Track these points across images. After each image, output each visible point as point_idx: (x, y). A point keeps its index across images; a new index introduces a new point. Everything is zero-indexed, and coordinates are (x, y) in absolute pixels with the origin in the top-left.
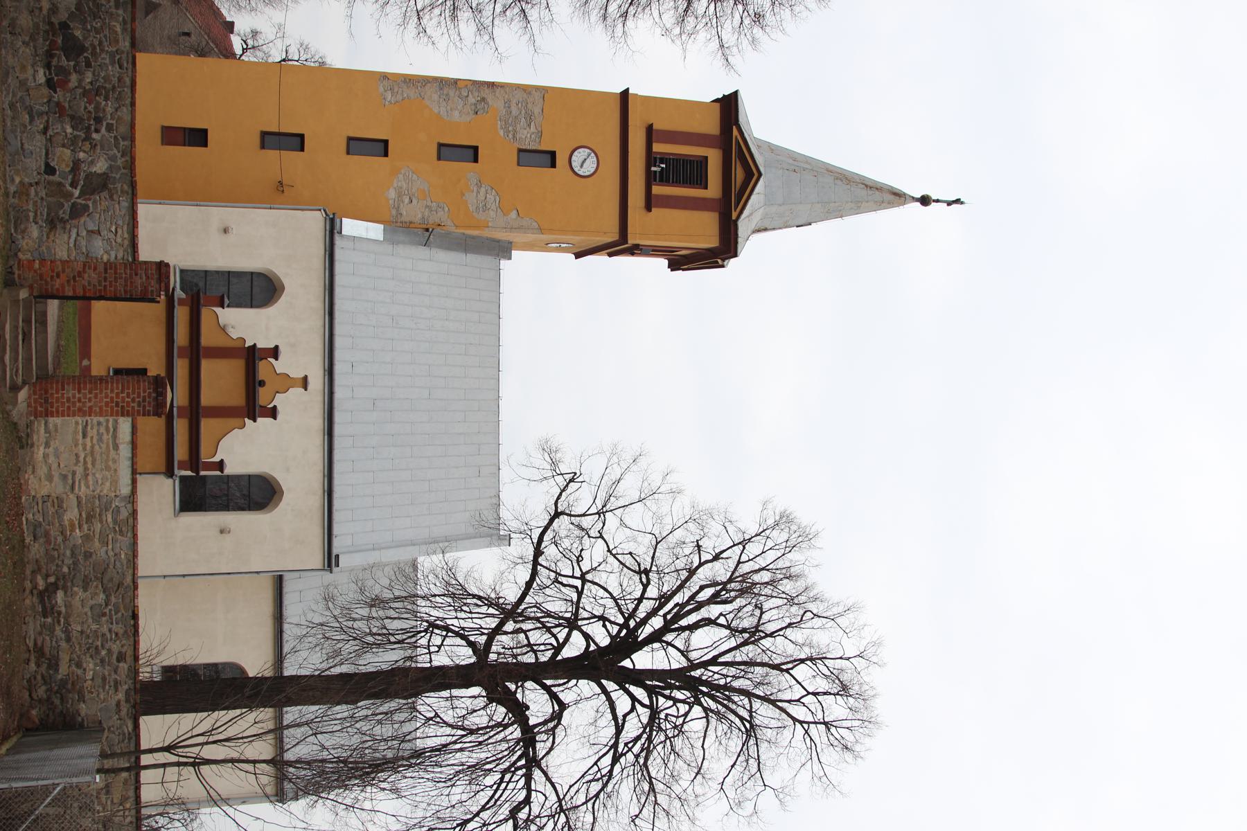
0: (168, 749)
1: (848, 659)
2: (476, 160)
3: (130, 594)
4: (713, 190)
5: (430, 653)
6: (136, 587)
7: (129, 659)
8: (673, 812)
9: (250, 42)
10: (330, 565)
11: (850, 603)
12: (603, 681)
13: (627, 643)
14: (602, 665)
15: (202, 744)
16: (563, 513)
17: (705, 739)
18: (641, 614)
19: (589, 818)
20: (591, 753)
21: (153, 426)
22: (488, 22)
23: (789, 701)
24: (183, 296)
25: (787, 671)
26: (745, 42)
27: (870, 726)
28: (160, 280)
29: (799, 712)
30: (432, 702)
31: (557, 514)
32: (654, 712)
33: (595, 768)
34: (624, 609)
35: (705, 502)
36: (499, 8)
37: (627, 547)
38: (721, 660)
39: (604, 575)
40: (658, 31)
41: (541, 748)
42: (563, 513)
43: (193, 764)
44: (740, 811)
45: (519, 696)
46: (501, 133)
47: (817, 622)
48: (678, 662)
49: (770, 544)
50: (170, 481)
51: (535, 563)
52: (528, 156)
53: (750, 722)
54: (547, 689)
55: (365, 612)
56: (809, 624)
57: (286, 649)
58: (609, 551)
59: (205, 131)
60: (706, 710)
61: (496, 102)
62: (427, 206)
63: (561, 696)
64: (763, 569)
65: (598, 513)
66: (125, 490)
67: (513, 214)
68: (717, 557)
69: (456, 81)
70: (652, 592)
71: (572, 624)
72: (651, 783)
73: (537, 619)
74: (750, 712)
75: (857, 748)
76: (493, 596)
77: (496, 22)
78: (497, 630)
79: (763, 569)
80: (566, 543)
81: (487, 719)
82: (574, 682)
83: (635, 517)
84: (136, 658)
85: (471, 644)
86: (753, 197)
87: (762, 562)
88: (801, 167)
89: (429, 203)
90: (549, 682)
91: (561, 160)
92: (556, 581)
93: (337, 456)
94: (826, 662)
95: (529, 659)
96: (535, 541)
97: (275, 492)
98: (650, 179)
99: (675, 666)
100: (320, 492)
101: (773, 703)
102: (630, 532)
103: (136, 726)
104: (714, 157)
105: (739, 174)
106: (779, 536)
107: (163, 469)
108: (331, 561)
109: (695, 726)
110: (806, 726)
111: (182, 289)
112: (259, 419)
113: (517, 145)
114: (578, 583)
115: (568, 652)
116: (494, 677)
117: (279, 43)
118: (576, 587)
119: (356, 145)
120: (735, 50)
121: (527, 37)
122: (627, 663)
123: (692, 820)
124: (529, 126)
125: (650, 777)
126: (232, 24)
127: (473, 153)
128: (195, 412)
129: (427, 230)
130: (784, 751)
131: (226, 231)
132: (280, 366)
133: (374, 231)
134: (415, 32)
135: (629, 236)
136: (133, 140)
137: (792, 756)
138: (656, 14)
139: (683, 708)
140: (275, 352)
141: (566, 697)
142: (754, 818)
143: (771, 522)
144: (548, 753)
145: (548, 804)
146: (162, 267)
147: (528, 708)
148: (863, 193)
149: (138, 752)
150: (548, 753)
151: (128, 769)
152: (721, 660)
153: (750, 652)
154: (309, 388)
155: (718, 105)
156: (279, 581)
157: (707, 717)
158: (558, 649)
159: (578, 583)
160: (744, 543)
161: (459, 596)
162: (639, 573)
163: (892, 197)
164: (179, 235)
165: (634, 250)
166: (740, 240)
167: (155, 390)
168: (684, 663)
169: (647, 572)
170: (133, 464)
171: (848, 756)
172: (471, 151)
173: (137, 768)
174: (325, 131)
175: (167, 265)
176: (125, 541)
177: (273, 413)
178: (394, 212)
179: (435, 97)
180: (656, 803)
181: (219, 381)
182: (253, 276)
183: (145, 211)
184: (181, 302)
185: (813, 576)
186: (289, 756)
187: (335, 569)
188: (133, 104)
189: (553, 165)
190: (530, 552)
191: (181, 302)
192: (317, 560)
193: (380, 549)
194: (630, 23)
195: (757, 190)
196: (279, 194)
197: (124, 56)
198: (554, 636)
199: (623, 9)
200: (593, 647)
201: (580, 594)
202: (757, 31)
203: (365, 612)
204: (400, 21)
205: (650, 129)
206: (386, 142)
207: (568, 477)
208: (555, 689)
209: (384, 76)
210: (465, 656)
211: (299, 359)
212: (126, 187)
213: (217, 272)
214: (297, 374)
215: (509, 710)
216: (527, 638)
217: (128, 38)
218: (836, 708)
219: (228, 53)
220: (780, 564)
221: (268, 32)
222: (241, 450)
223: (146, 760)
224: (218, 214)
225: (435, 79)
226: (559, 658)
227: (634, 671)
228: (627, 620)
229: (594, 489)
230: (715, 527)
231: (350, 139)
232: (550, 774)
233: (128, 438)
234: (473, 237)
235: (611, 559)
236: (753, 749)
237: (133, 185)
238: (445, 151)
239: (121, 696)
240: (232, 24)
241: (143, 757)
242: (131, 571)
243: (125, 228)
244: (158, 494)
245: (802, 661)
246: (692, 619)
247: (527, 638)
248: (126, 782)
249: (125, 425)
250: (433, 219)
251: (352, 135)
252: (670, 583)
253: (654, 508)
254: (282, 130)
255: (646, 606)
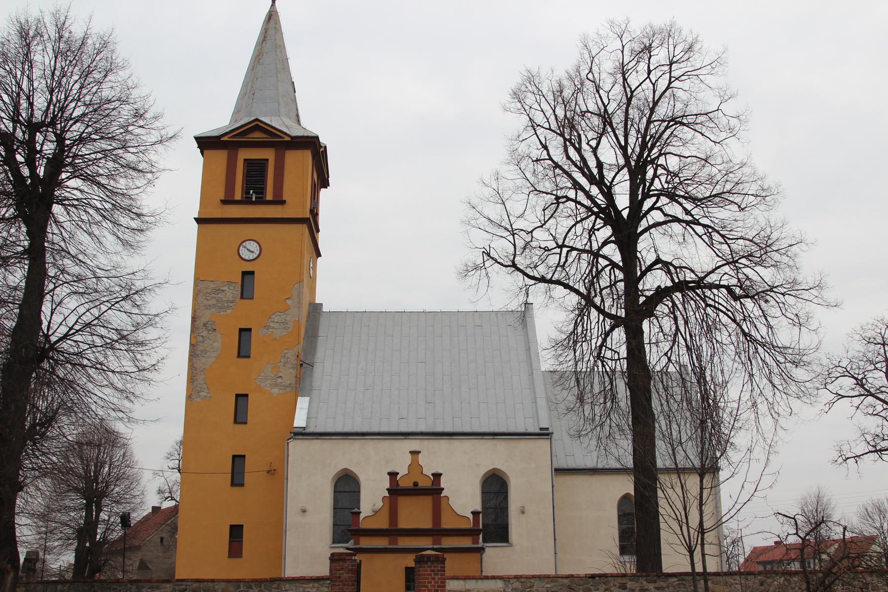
0: (691, 552)
1: (623, 47)
2: (250, 330)
3: (576, 580)
4: (268, 154)
5: (619, 359)
6: (572, 576)
7: (624, 580)
8: (736, 180)
9: (167, 495)
10: (548, 434)
11: (581, 45)
12: (640, 230)
13: (608, 213)
14: (626, 233)
15: (688, 527)
16: (513, 261)
17: (681, 154)
18: (587, 202)
19: (741, 242)
20: (691, 240)
21: (452, 564)
22: (146, 319)
23: (654, 92)
24: (352, 541)
25: (632, 92)
26: (157, 124)
27: (673, 31)
28: (344, 560)
29: (662, 85)
30: (654, 357)
31: (514, 265)
32: (662, 193)
33: (704, 237)
34: (584, 215)
35: (504, 155)
36: (135, 311)
37: (539, 212)
38: (623, 143)
39: (559, 230)
40: (149, 189)
41: (690, 276)
42: (513, 261)
43: (703, 533)
44: (737, 129)
45: (648, 294)
46: (229, 311)
47: (595, 69)
48: (625, 174)
49: (536, 106)
50: (487, 550)
51: (550, 281)
52: (246, 293)
53: (669, 122)
54: (644, 274)
55: (587, 408)
56: (597, 76)
57: (619, 466)
58: (541, 227)
59: (232, 527)
60: (660, 155)
61: (206, 316)
62: (284, 365)
63: (648, 263)
64: (554, 111)
65: (513, 235)
66: (500, 584)
67: (289, 302)
68: (545, 147)
69: (192, 345)
70: (571, 194)
71: (596, 255)
72: (715, 196)
73: (593, 278)
74: (663, 121)
75: (690, 40)
76: (577, 312)
77: (146, 312)
78: (601, 311)
79: (554, 111)
80: (535, 259)
81: (667, 318)
82: (639, 255)
83: (516, 206)
84: (624, 576)
85: (612, 329)
86: (273, 125)
87: (549, 112)
88: (250, 89)
89: (282, 364)
90: (639, 273)
91: (248, 267)
92: (563, 266)
93: (467, 429)
94: (625, 63)
95: (621, 286)
96: (533, 282)
97: (494, 474)
98: (261, 201)
99: (627, 177)
100: (494, 442)
101: (655, 103)
102: (528, 211)
103: (674, 575)
104: (244, 154)
105: (257, 136)
106: (530, 99)
107: (477, 555)
108: (544, 434)
109: (673, 163)
110: (673, 79)
111: (347, 542)
112: (442, 486)
113: (238, 300)
114: (565, 250)
115: (617, 258)
116: (636, 312)
117: (167, 474)
118: (568, 252)
119: (240, 417)
120: (163, 132)
121: (157, 289)
122: (625, 214)
123: (743, 165)
124: (223, 291)
125: (710, 196)
126: (153, 508)
127: (244, 332)
128: (437, 532)
129: (301, 365)
130: (694, 95)
131: (304, 511)
132: (403, 471)
133: (303, 404)
134: (154, 372)
135: (305, 217)
136: (239, 581)
137: (696, 90)
138: (137, 191)
139: (660, 171)
140: (393, 475)
141: (650, 258)
142: (742, 118)
143: (519, 105)
144: (693, 271)
145: (731, 273)
146: (334, 559)
147: (659, 287)
148: (269, 44)
149: (693, 574)
150: (693, 271)
151: (706, 582)
152: (623, 143)
153: (618, 119)
154: (418, 450)
155: (206, 152)
156: (559, 471)
157: (665, 154)
158: (613, 265)
159: (565, 250)
160: (534, 126)
161: (573, 340)
162: (558, 203)
163: (272, 21)
164: (308, 548)
165: (314, 213)
166: (306, 134)
167: (426, 562)
168: (626, 170)
169: (558, 198)
170: (474, 578)
171: (696, 47)
172: (243, 333)
173: (705, 575)
174: (231, 440)
175: (332, 555)
176: (537, 584)
177: (437, 476)
178: (289, 389)
179: (203, 360)
180: (729, 192)
181: (414, 515)
182: (337, 491)
183: (291, 570)
184: (357, 543)
185: (560, 73)
186: (697, 463)
187: (550, 431)
188: (213, 581)
189: (252, 273)
190: (542, 286)
191: (357, 543)
192: (544, 444)
193: (536, 398)
194: (144, 212)
195: (268, 122)
196: (276, 473)
197: (177, 588)
198: (603, 269)
199: (133, 216)
200: (613, 238)
201: (573, 249)
202: (148, 116)
203: (587, 408)
204: (146, 384)
205: (224, 202)
206: (237, 396)
207: (486, 258)
208: (643, 269)
209: (189, 397)
210: (619, 335)
211: (397, 455)
212: (275, 586)
213: (334, 517)
214: (408, 459)
215: (661, 301)
216: (606, 288)
217: (164, 585)
218: (660, 56)
219: (175, 510)
220: (550, 98)
221: (159, 482)
222: (464, 499)
223: (699, 568)
224: (292, 517)
225: (190, 360)
226: (621, 264)
227: (631, 207)
228: (593, 213)
229: (495, 238)
230: (522, 148)
231: (235, 422)
232: (710, 269)
233: (461, 582)
234: (306, 331)
235: (547, 226)
236: (691, 119)
237: (273, 580)
238: (243, 352)
239: (651, 586)
240: (153, 508)
241: (697, 570)
242: (560, 580)
243: (305, 586)
244: (495, 559)
245: (625, 80)
246: (592, 163)
247: (606, 288)
248: (713, 583)
249: (451, 585)
250: (293, 360)
251: (232, 420)
252: (565, 182)
253: (510, 192)
254: (230, 470)
255: (581, 197)
